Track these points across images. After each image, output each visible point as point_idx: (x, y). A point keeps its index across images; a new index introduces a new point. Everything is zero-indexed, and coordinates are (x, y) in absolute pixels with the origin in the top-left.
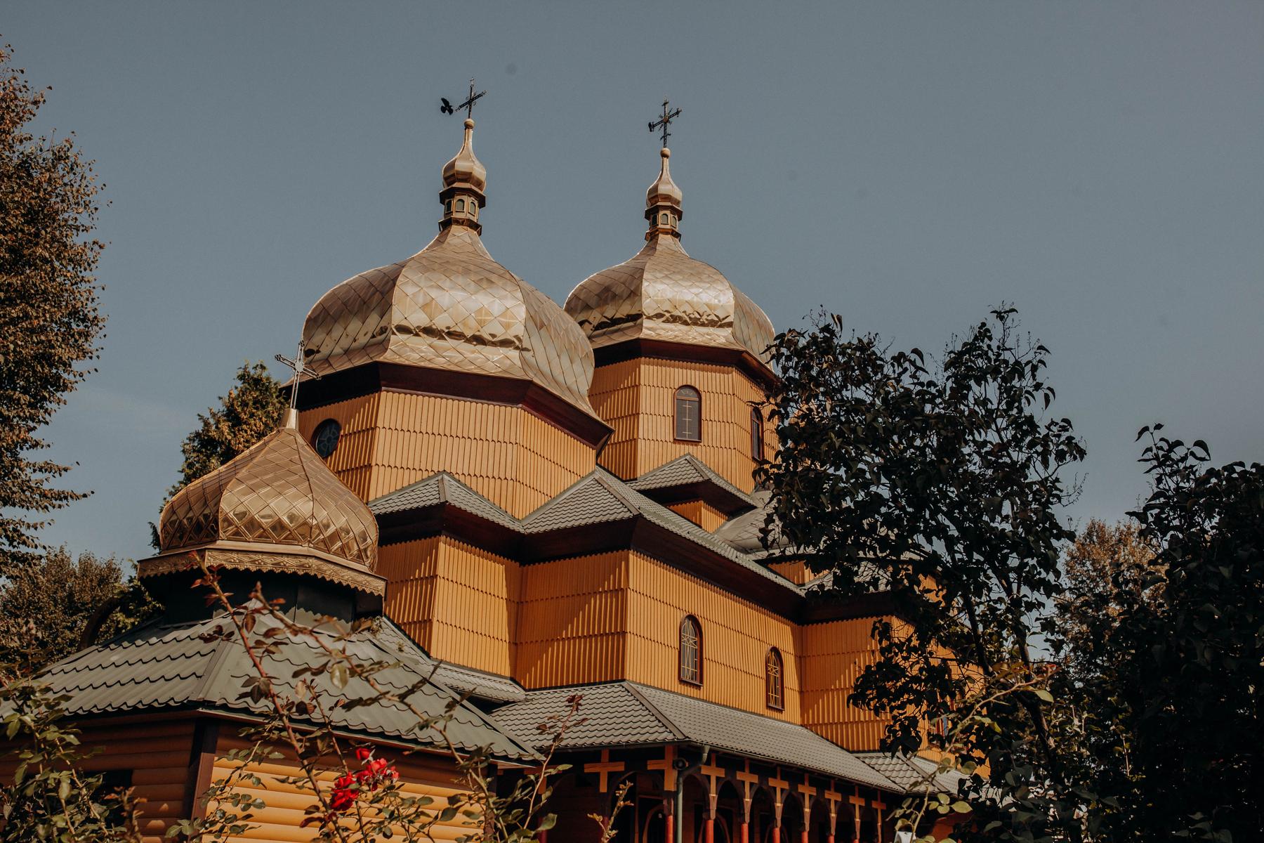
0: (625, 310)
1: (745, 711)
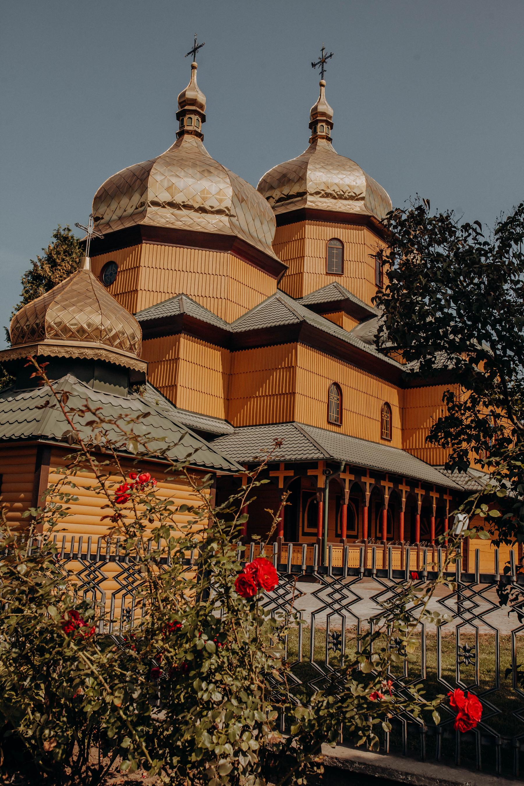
0: (296, 189)
1: (368, 441)
